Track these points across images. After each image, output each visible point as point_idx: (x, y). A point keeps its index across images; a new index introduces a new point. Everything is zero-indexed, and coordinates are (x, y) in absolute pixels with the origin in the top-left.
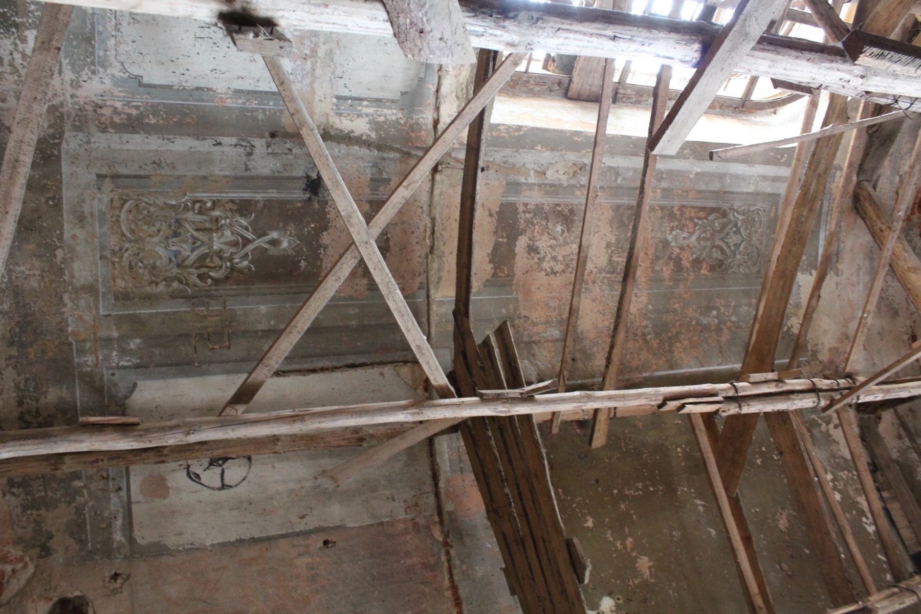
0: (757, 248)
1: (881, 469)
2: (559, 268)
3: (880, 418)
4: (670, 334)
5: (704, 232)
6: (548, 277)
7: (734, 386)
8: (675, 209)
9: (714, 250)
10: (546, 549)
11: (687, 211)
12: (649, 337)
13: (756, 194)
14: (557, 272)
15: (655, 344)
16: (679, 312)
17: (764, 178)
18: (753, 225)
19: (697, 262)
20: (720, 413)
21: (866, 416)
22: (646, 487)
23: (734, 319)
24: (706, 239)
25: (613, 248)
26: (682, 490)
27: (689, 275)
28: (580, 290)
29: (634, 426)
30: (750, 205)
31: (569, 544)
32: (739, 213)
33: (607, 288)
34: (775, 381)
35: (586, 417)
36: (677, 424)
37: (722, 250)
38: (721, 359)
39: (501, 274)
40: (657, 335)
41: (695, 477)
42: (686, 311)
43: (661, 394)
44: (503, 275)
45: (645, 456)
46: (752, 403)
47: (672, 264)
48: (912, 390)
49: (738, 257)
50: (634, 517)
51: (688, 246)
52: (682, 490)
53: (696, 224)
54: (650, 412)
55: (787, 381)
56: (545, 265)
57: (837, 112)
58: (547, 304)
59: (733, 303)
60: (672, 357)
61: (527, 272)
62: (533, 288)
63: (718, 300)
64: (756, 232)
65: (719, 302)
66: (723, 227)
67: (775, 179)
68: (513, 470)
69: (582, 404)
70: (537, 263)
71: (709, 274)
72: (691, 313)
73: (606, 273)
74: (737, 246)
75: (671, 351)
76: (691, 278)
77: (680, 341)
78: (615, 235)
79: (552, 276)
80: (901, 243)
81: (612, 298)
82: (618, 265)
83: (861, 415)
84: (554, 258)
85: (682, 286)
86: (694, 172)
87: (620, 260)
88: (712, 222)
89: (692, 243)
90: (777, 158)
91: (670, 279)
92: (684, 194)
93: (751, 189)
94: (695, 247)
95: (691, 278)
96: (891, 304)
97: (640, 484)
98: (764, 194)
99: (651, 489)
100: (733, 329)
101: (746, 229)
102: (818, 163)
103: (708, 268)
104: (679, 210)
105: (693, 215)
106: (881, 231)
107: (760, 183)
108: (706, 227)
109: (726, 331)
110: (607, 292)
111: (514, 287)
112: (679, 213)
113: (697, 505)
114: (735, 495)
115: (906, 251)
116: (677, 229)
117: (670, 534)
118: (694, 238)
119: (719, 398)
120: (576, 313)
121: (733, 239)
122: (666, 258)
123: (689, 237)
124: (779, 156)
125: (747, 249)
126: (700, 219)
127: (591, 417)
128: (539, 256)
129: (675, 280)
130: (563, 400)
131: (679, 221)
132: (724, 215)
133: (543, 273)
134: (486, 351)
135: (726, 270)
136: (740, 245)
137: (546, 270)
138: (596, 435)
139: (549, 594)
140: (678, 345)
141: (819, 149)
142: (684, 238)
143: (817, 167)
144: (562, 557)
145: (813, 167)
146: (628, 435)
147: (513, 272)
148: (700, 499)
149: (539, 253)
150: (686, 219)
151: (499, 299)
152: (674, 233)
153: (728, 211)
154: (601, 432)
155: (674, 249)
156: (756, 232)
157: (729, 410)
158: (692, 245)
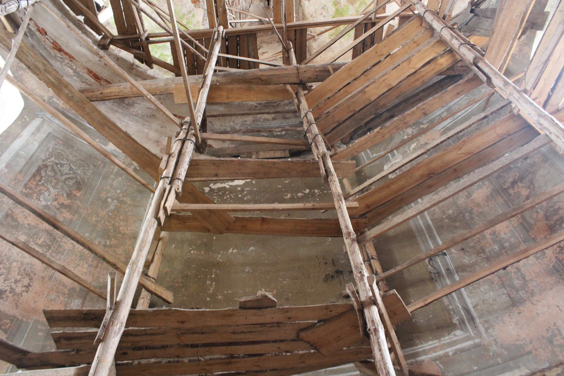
0: (79, 160)
1: (239, 153)
2: (26, 281)
3: (210, 146)
4: (112, 230)
5: (51, 182)
6: (29, 292)
7: (163, 177)
8: (24, 191)
9: (67, 183)
10: (241, 332)
11: (30, 185)
12: (108, 243)
13: (42, 143)
14: (29, 284)
15: (114, 242)
16: (99, 219)
17: (33, 134)
18: (62, 155)
19: (69, 195)
20: (178, 191)
21: (207, 151)
22: (211, 279)
23: (118, 191)
24: (57, 183)
25: (31, 240)
26: (220, 258)
27: (76, 204)
28: (49, 259)
29: (166, 273)
30: (48, 150)
31: (244, 306)
32: (50, 158)
33: (59, 255)
34: (169, 157)
35: (149, 298)
36: (174, 247)
37: (69, 178)
38: (142, 208)
39: (7, 326)
40: (109, 238)
41: (213, 248)
42: (100, 215)
43: (151, 218)
44: (9, 324)
45: (189, 273)
46: (179, 171)
47: (63, 210)
48: (202, 101)
49: (79, 172)
50: (229, 292)
51: (55, 195)
52: (220, 258)
53: (43, 184)
54: (161, 257)
55: (172, 152)
56: (18, 290)
57: (6, 38)
58: (51, 300)
59: (108, 188)
60: (128, 235)
61: (17, 306)
62: (33, 306)
63: (102, 195)
64: (68, 155)
65: (103, 195)
66: (53, 170)
67: (38, 129)
68: (171, 346)
69: (137, 269)
70: (13, 295)
71: (82, 192)
72: (103, 213)
73: (48, 251)
74: (71, 169)
75: (124, 235)
76: (79, 204)
77: (119, 227)
78: (22, 234)
79: (30, 288)
80: (114, 86)
81: (68, 255)
82: (46, 242)
83: (205, 153)
84: (16, 282)
85: (82, 211)
86: (4, 168)
87: (42, 239)
88: (46, 175)
89: (55, 192)
90: (24, 122)
91: (73, 215)
92: (17, 181)
93: (36, 145)
94: (59, 192)
95: (79, 204)
96: (147, 116)
97: (208, 282)
98: (44, 140)
99: (213, 276)
100: (125, 194)
101: (63, 160)
102: (36, 67)
103: (77, 191)
104: (26, 189)
105: (35, 183)
106: (101, 93)
107: (36, 138)
108: (48, 180)
109: (125, 199)
110: (62, 257)
111: (24, 320)
112: (28, 190)
113: (232, 252)
114: (234, 219)
115: (120, 86)
116: (40, 196)
117: (247, 273)
118: (52, 190)
119: (168, 187)
120: (66, 270)
121: (66, 169)
122: (57, 211)
123: (50, 192)
124: (23, 120)
125: (77, 165)
126: (40, 181)
127: (150, 294)
128: (8, 292)
129: (75, 212)
130: (129, 281)
131: (34, 192)
132: (46, 166)
133: (24, 294)
134: (64, 342)
135: (84, 182)
136: (71, 167)
137: (23, 291)
138: (164, 296)
139: (275, 341)
140: (121, 228)
141: (27, 63)
142: (49, 195)
143: (39, 69)
144: (253, 317)
145: (37, 72)
146: (172, 279)
147: (11, 316)
148: (229, 250)
149: (6, 291)
150: (36, 188)
151: (28, 335)
152: (41, 199)
153: (44, 163)
154: (163, 292)
155: (53, 204)
156: (68, 155)
157: (178, 186)
158: (56, 193)
